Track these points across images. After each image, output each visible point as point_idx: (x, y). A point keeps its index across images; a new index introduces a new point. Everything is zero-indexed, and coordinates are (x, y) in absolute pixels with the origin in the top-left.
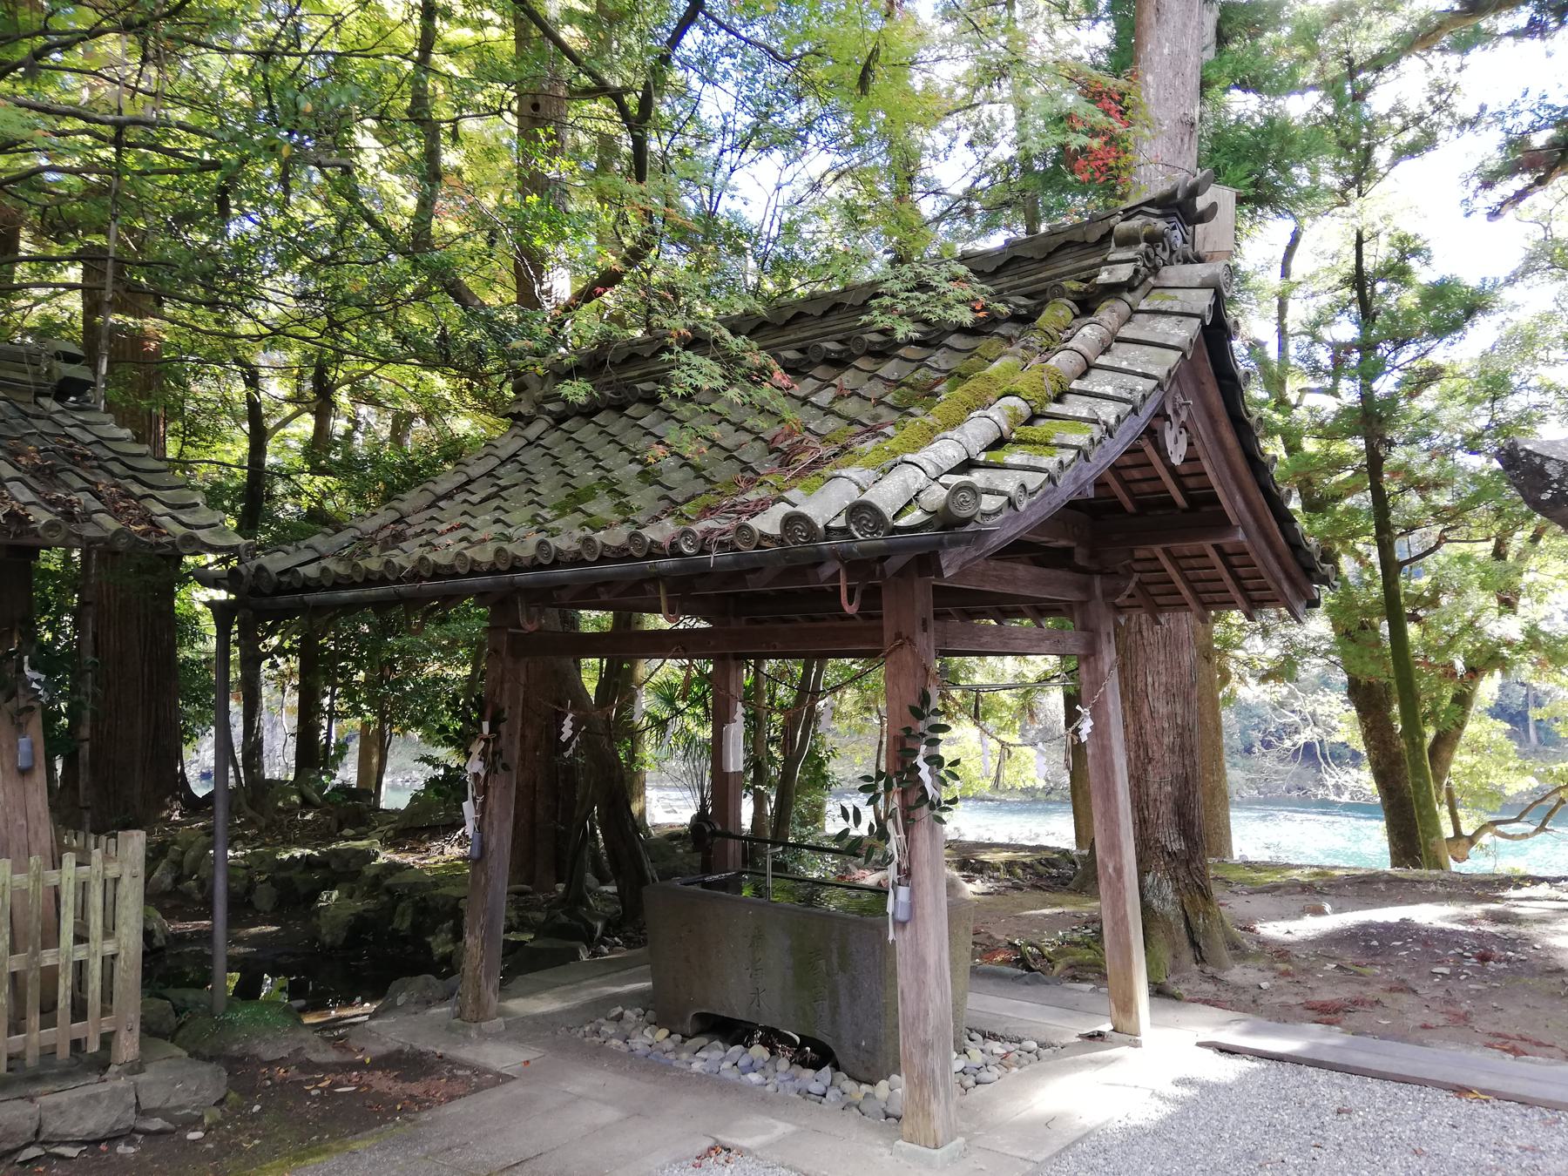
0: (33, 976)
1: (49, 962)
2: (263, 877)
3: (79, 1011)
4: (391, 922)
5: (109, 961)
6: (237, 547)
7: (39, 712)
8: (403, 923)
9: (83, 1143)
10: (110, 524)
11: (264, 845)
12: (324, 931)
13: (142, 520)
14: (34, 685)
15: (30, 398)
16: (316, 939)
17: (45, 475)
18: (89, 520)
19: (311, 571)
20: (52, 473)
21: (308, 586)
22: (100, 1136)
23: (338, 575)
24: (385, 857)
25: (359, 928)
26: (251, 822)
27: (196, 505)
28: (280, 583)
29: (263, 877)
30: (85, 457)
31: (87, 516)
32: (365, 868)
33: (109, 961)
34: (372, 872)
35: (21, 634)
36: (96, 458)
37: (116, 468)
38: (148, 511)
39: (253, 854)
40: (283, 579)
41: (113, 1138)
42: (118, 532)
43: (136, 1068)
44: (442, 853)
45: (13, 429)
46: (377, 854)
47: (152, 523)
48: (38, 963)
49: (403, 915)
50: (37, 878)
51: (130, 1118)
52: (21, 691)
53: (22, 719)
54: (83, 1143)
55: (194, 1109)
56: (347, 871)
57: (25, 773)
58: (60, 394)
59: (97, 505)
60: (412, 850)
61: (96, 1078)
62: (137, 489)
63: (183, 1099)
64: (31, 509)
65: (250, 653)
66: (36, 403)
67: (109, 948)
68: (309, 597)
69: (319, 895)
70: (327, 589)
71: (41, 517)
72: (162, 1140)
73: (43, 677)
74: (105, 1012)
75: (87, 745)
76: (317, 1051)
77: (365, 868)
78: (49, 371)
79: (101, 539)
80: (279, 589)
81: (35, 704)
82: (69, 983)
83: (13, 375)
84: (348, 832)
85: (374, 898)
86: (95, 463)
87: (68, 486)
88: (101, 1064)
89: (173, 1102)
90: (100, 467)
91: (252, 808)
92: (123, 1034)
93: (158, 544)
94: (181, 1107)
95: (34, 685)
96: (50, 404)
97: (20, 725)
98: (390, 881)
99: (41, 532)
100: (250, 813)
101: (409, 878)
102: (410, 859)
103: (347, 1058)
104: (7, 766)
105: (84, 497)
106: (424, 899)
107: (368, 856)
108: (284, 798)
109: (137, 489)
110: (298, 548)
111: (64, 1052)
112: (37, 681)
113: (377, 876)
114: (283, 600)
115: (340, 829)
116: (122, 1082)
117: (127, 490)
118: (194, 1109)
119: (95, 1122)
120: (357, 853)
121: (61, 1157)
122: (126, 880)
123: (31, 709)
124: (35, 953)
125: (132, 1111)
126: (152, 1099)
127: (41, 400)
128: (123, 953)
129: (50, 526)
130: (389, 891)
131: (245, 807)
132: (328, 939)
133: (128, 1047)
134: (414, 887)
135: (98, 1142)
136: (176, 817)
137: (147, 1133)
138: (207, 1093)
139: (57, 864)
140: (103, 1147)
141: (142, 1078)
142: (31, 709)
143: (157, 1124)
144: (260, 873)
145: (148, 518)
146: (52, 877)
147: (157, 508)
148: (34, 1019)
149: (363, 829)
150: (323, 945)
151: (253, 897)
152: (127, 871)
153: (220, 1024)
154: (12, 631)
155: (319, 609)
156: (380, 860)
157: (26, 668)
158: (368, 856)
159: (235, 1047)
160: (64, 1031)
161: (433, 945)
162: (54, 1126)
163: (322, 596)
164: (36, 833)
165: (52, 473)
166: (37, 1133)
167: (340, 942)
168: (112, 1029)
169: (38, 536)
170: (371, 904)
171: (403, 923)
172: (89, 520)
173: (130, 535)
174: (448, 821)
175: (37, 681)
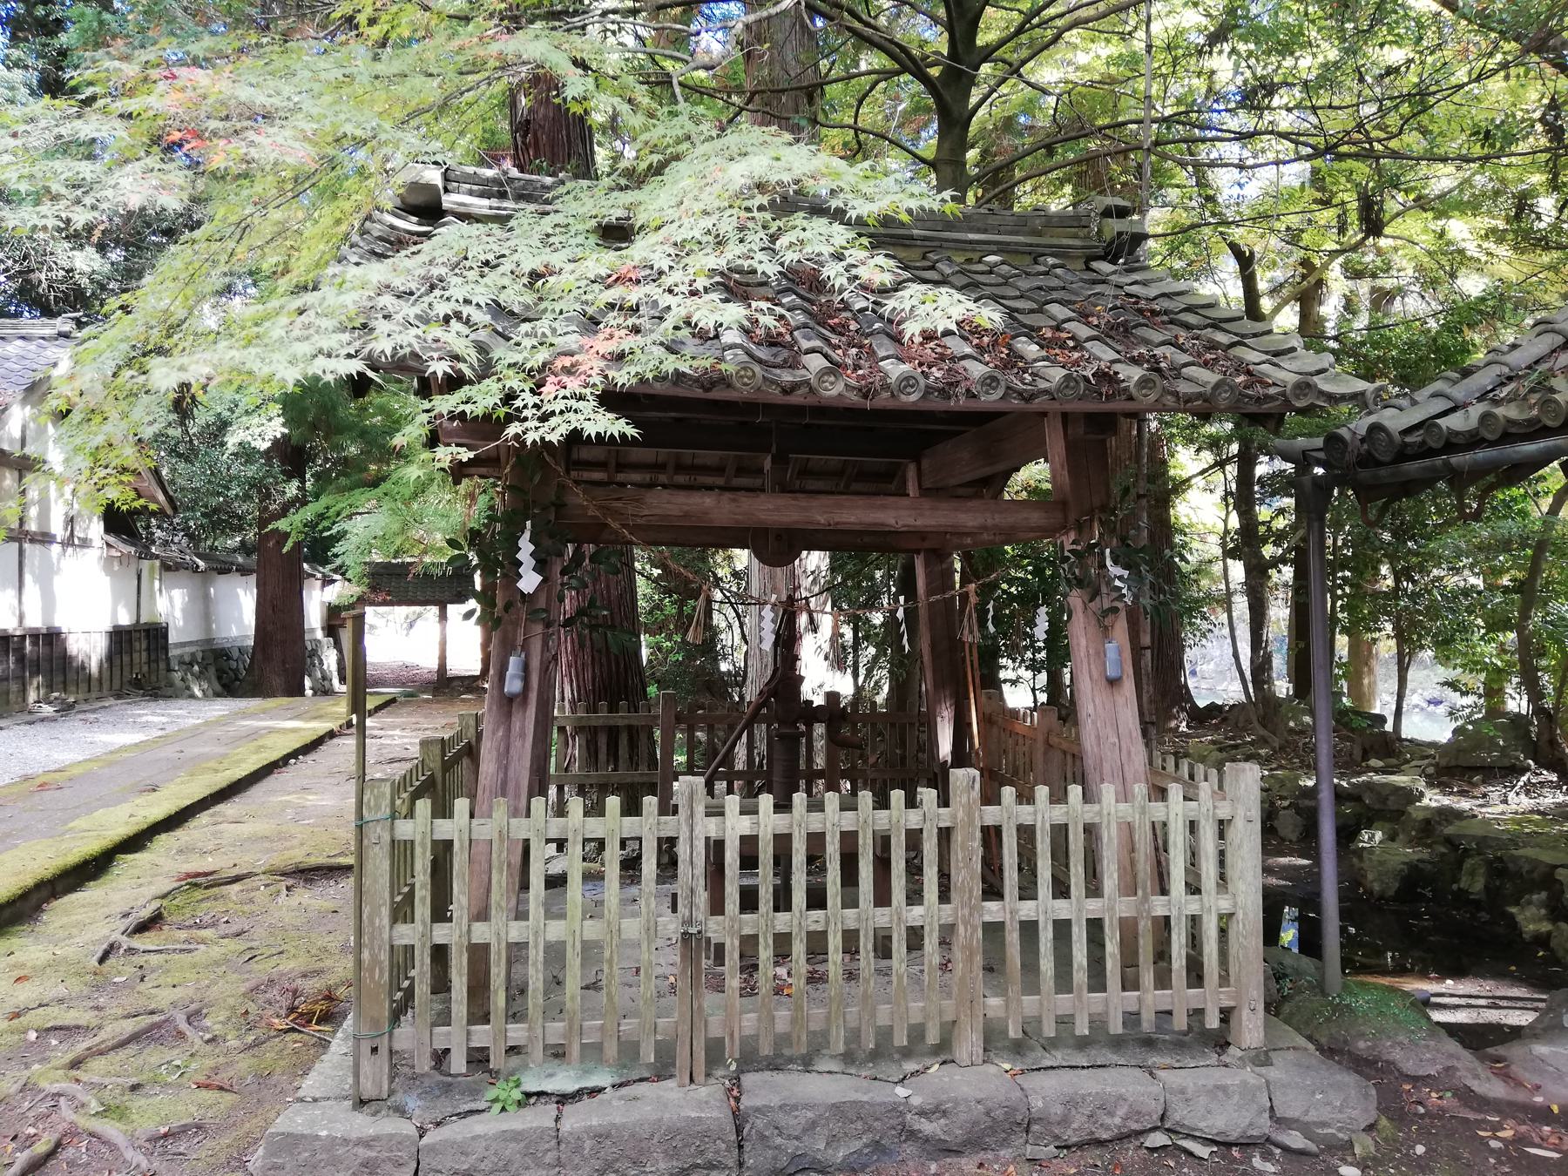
0: (1145, 926)
1: (1160, 912)
2: (1286, 803)
3: (1195, 974)
4: (1456, 880)
5: (1226, 919)
6: (1363, 393)
7: (1123, 614)
8: (1474, 883)
9: (1213, 1142)
10: (1209, 377)
11: (1280, 767)
12: (1370, 876)
13: (1238, 372)
14: (1117, 583)
15: (1080, 265)
16: (1360, 884)
17: (1118, 332)
18: (1178, 376)
19: (1455, 422)
20: (1126, 330)
21: (1454, 443)
22: (1231, 1139)
23: (1510, 421)
24: (1433, 799)
25: (1413, 878)
26: (1263, 742)
27: (1293, 349)
28: (1406, 445)
29: (1286, 803)
30: (1153, 312)
31: (1176, 371)
32: (1410, 809)
33: (1226, 919)
34: (1420, 816)
35: (1102, 523)
36: (1166, 312)
37: (1191, 319)
38: (1241, 361)
39: (1271, 776)
40: (1408, 439)
41: (1247, 1145)
42: (1217, 386)
43: (1262, 1059)
44: (1505, 802)
45: (1077, 294)
46: (1422, 794)
47: (1249, 373)
48: (1149, 912)
49: (1472, 874)
50: (1143, 812)
51: (1264, 1125)
52: (1104, 589)
53: (1107, 622)
54: (1213, 1142)
55: (1340, 1129)
56: (1391, 809)
57: (1113, 683)
58: (1111, 255)
59: (1185, 358)
60: (1463, 793)
61: (1213, 1058)
62: (1222, 338)
63: (1324, 1114)
64: (1117, 367)
65: (1254, 561)
66: (1089, 269)
67: (1225, 905)
68: (1456, 459)
69: (1358, 832)
70: (1492, 444)
71: (1131, 374)
72: (1309, 1161)
73: (1126, 573)
74: (1224, 980)
75: (1148, 653)
76: (1476, 1077)
77: (1410, 809)
78: (1100, 231)
79: (1200, 395)
80: (1403, 454)
81: (1120, 605)
82: (1184, 941)
83: (1065, 242)
84: (1374, 762)
85: (1428, 846)
86: (1165, 318)
87: (1146, 342)
88: (1220, 1042)
89: (1313, 1116)
90: (1171, 322)
91: (1265, 727)
92: (1245, 1013)
93: (1267, 396)
94: (1324, 1124)
95: (1117, 583)
96: (1104, 267)
97: (1106, 628)
98: (1449, 830)
99: (1133, 391)
100: (1263, 732)
101: (1475, 830)
102: (1465, 804)
103: (1520, 1096)
104: (1095, 675)
105: (1168, 351)
106: (1500, 859)
107: (1411, 796)
108: (1294, 718)
109: (1222, 338)
110: (1414, 403)
111: (1180, 1022)
112: (1120, 578)
113: (1427, 822)
114: (1413, 467)
115: (1365, 757)
116: (1248, 1075)
117: (1210, 341)
118: (1340, 1129)
119: (1228, 1119)
120: (1397, 790)
121: (1190, 1154)
122: (1239, 823)
123: (1115, 610)
124: (1145, 899)
125: (1267, 1115)
126: (1291, 1107)
127: (1095, 265)
128: (1240, 914)
129: (1144, 383)
130: (1449, 841)
131: (1256, 724)
132: (1376, 887)
133: (1252, 1028)
134: (1483, 842)
135: (1229, 1145)
136: (1183, 727)
137: (1286, 1149)
138: (1355, 1114)
139: (1160, 793)
140: (1235, 1152)
141: (1273, 1073)
142: (1115, 610)
143: (1296, 1140)
144: (1282, 798)
145: (1243, 368)
146: (1157, 810)
147: (1252, 356)
148: (1148, 977)
149: (1394, 761)
150: (1370, 893)
151: (1276, 823)
152: (1241, 812)
153: (1336, 1008)
154: (1091, 521)
155: (1477, 473)
156: (1425, 801)
157: (1109, 562)
158: (1411, 796)
159: (1362, 1044)
160: (1180, 997)
161: (1519, 918)
162: (1179, 1114)
163: (1481, 455)
164: (1129, 753)
165: (1126, 330)
166: (1162, 1118)
167: (1391, 893)
168: (1232, 1004)
169: (1131, 398)
170: (1425, 853)
171: (1474, 883)
172: (1178, 376)
173: (1232, 388)
174: (1506, 762)
175: (1120, 578)
